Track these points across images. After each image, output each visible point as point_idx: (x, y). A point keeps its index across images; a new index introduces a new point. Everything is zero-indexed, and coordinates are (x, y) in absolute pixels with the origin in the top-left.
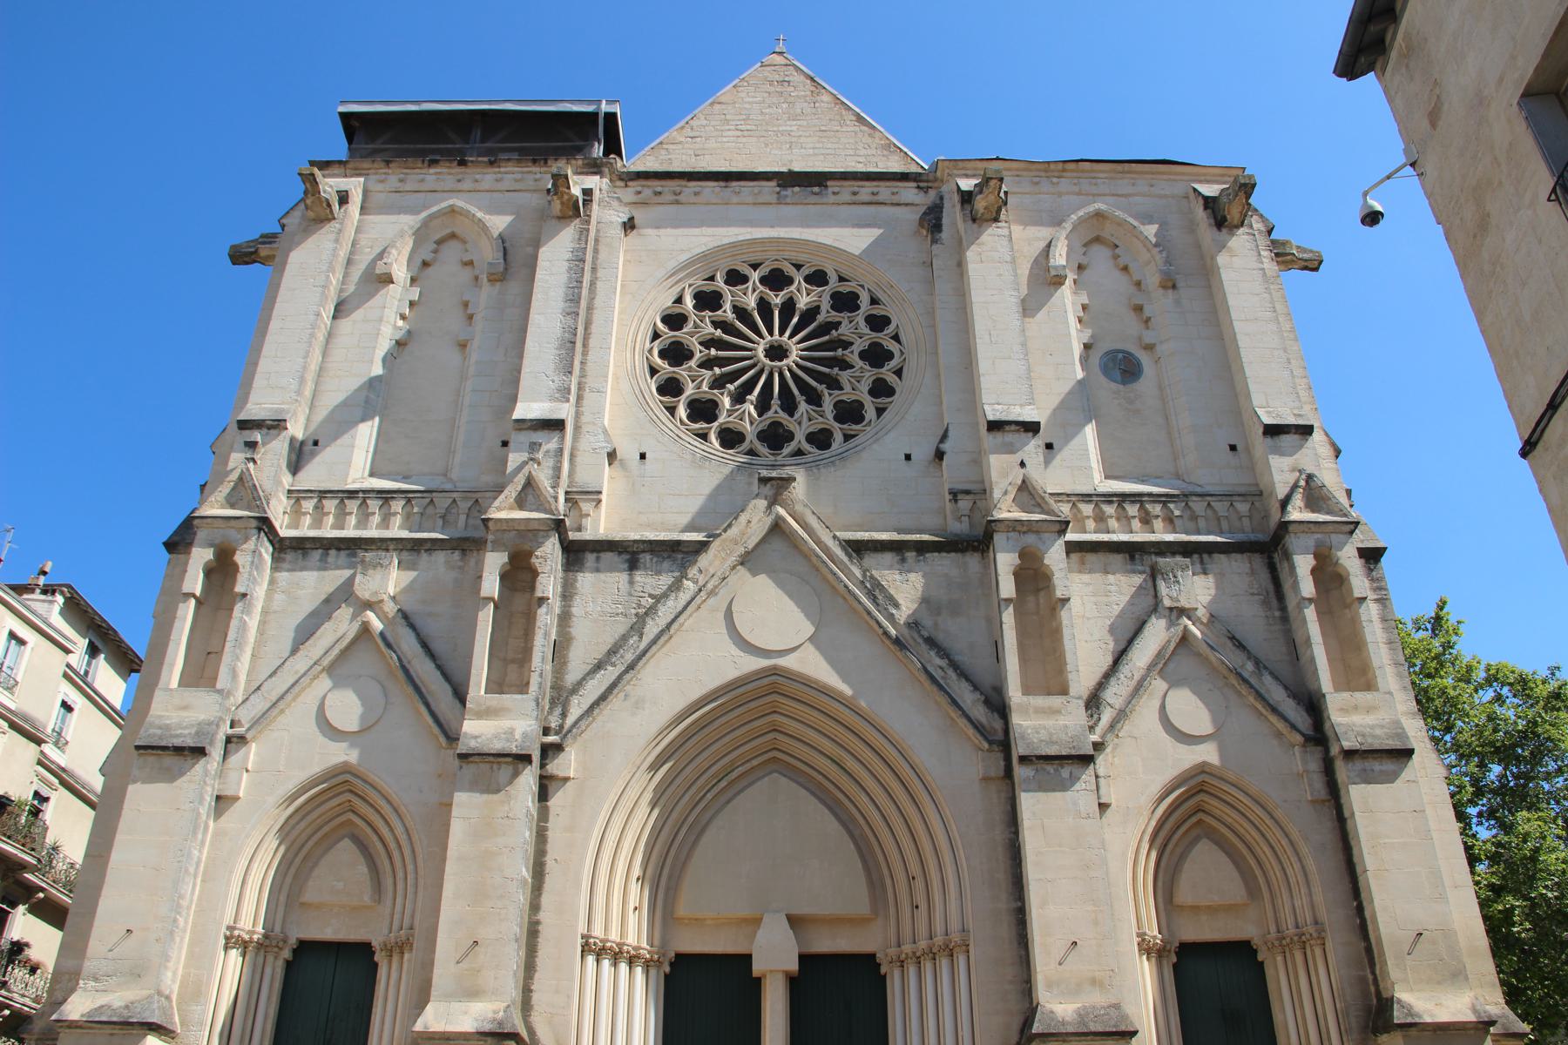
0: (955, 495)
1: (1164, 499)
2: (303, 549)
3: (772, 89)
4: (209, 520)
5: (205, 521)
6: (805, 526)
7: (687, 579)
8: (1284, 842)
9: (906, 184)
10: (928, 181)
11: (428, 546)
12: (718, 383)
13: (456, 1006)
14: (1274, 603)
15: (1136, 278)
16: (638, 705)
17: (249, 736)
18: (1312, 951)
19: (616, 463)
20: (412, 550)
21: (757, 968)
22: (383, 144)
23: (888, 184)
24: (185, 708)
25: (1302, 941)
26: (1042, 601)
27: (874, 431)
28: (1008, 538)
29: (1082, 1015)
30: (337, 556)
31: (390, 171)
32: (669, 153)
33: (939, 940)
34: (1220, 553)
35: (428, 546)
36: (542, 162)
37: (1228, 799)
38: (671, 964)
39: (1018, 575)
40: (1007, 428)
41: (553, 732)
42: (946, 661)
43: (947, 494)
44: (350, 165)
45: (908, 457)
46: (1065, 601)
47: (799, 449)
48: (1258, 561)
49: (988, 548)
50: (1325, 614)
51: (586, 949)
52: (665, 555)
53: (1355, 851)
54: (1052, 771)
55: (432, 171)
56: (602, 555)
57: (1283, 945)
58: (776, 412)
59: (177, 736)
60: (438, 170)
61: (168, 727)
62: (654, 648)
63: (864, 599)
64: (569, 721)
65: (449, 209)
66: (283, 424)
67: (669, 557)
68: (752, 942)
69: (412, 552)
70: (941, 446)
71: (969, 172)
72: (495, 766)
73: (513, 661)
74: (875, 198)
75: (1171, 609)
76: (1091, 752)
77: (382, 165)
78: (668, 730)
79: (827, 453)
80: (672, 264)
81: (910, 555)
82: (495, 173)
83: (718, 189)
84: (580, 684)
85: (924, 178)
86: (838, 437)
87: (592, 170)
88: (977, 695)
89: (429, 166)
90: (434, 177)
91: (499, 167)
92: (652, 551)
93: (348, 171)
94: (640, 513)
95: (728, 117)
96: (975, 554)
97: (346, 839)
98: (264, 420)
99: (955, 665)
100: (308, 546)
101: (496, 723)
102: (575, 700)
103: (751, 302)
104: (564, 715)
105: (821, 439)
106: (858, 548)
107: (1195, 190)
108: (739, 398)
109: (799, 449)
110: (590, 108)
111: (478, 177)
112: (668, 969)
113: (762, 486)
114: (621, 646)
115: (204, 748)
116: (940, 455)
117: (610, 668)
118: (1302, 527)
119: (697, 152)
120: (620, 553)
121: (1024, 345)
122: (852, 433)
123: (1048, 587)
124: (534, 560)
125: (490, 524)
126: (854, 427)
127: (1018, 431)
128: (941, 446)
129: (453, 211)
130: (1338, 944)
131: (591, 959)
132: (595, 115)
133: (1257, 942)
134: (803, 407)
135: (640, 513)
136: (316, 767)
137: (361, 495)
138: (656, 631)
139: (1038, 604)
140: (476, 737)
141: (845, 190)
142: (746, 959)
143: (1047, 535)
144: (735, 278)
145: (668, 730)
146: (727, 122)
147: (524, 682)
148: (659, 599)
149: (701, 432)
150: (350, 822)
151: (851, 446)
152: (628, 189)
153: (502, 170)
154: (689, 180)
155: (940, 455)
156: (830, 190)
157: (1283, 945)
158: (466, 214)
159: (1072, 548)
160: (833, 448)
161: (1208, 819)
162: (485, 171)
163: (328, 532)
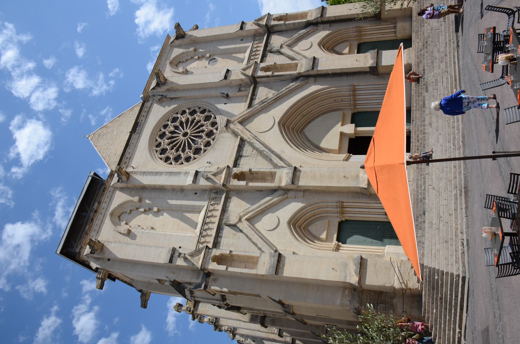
2: (216, 243)
3: (101, 138)
4: (203, 263)
5: (203, 265)
6: (242, 117)
8: (338, 32)
9: (145, 104)
10: (146, 100)
11: (224, 207)
12: (177, 150)
13: (361, 180)
14: (283, 32)
15: (135, 208)
17: (275, 249)
18: (345, 211)
20: (224, 212)
22: (89, 209)
23: (144, 108)
24: (264, 264)
25: (360, 31)
29: (372, 58)
31: (90, 234)
32: (112, 162)
33: (351, 93)
34: (268, 41)
35: (224, 207)
36: (105, 189)
37: (326, 42)
39: (239, 180)
40: (227, 75)
44: (83, 246)
46: (250, 170)
50: (252, 180)
53: (343, 18)
55: (95, 221)
56: (238, 164)
57: (360, 36)
58: (203, 135)
59: (274, 262)
60: (95, 219)
61: (270, 267)
63: (265, 103)
66: (174, 249)
69: (225, 212)
71: (148, 88)
72: (296, 176)
74: (147, 112)
75: (280, 48)
76: (277, 253)
77: (87, 235)
80: (150, 159)
81: (254, 97)
82: (103, 203)
83: (130, 147)
85: (145, 100)
86: (212, 141)
87: (112, 177)
89: (93, 222)
90: (97, 221)
91: (101, 202)
92: (240, 152)
94: (225, 162)
95: (106, 148)
98: (171, 254)
100: (216, 241)
101: (284, 178)
103: (172, 129)
105: (208, 144)
106: (250, 106)
107: (171, 43)
108: (183, 151)
110: (90, 178)
111: (102, 208)
118: (267, 22)
119: (115, 155)
120: (238, 159)
121: (204, 74)
124: (238, 173)
125: (224, 183)
130: (362, 24)
132: (93, 178)
133: (353, 112)
134: (204, 128)
135: (225, 162)
136: (288, 231)
138: (263, 147)
140: (287, 181)
141: (142, 118)
144: (165, 126)
146: (107, 148)
148: (254, 148)
150: (304, 228)
152: (131, 145)
153: (102, 201)
154: (124, 155)
156: (140, 122)
157: (360, 36)
158: (114, 210)
159: (262, 61)
160: (212, 144)
161: (330, 48)
162: (101, 206)
163: (213, 233)
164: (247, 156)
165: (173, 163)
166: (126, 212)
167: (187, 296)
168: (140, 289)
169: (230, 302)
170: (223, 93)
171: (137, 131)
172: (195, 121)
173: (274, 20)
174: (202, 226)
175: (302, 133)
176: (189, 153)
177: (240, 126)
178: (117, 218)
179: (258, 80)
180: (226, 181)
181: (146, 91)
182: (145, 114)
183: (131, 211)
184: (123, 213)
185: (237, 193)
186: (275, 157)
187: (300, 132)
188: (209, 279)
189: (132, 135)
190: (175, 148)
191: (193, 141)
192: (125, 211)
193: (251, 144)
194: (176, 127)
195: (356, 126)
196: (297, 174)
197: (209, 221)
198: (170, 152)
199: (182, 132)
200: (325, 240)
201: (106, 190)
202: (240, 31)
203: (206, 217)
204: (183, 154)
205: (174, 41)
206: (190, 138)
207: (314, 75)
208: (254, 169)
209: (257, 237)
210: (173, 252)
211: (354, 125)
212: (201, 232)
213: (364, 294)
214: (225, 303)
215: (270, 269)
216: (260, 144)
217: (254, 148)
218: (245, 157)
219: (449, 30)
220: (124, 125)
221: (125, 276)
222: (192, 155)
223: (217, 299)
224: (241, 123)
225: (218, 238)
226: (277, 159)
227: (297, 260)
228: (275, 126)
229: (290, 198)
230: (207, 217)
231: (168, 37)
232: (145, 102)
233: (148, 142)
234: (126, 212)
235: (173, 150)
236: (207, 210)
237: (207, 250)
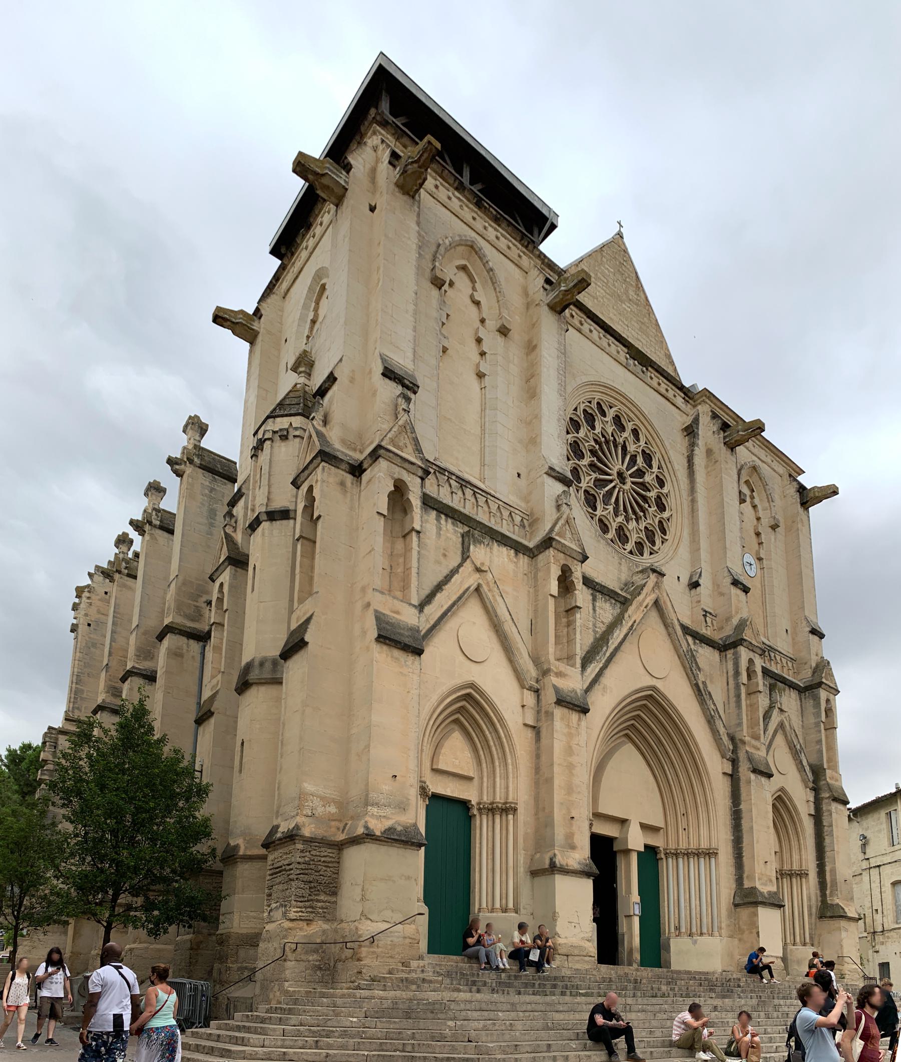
1: (464, 483)
4: (391, 455)
5: (388, 454)
10: (689, 397)
11: (499, 539)
24: (398, 613)
30: (446, 521)
52: (607, 598)
59: (400, 634)
65: (469, 243)
72: (571, 712)
89: (457, 189)
91: (499, 225)
93: (397, 143)
106: (686, 630)
115: (383, 374)
129: (472, 247)
136: (458, 681)
137: (447, 474)
148: (611, 628)
164: (594, 610)
165: (570, 436)
166: (474, 289)
167: (274, 422)
168: (263, 312)
169: (266, 532)
170: (700, 575)
171: (631, 362)
172: (646, 506)
173: (828, 701)
174: (457, 477)
175: (624, 739)
176: (588, 478)
177: (650, 600)
178: (463, 262)
179: (730, 653)
181: (709, 398)
182: (662, 389)
183: (477, 303)
184: (473, 281)
185: (525, 574)
186: (597, 670)
187: (627, 735)
188: (345, 471)
189: (624, 346)
190: (597, 447)
191: (610, 493)
192: (478, 285)
193: (617, 621)
194: (633, 459)
195: (639, 853)
196: (574, 712)
197: (467, 497)
198: (588, 434)
199: (628, 469)
200: (434, 767)
201: (523, 245)
202: (809, 629)
203: (476, 490)
204: (585, 466)
205: (795, 483)
206: (614, 487)
207: (738, 772)
208: (581, 619)
209: (445, 607)
210: (407, 383)
212: (445, 470)
213: (329, 851)
214: (264, 517)
215: (387, 623)
216: (619, 640)
217: (611, 628)
218: (593, 604)
219: (401, 1047)
220: (640, 333)
221: (300, 272)
223: (271, 497)
224: (656, 603)
225: (435, 512)
226: (593, 676)
227: (408, 692)
228: (648, 677)
229: (522, 694)
230: (475, 492)
231: (797, 470)
232: (685, 393)
233: (609, 382)
234: (474, 289)
235: (593, 443)
236: (489, 496)
237: (420, 473)
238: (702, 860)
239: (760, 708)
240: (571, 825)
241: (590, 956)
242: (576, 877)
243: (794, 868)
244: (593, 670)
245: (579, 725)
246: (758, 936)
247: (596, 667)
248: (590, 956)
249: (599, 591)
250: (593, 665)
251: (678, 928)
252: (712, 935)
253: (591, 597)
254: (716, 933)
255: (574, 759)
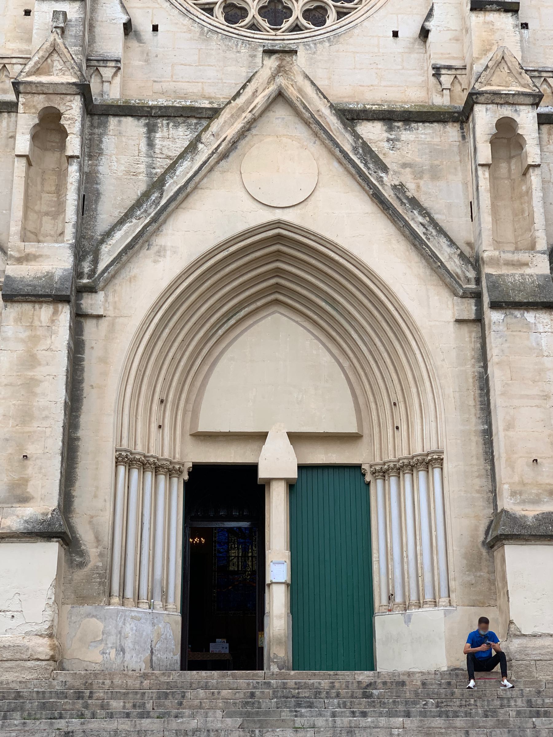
0: (437, 71)
7: (202, 143)
16: (161, 253)
19: (132, 34)
21: (262, 474)
26: (513, 167)
27: (366, 8)
28: (487, 109)
38: (190, 474)
41: (86, 276)
42: (428, 218)
43: (430, 68)
45: (395, 34)
47: (254, 24)
48: (280, 99)
49: (468, 118)
51: (119, 460)
52: (180, 120)
54: (519, 315)
62: (173, 205)
64: (101, 266)
67: (184, 123)
68: (259, 455)
70: (427, 24)
72: (37, 306)
73: (47, 214)
78: (186, 275)
79: (322, 30)
84: (108, 234)
86: (332, 14)
88: (453, 250)
94: (155, 81)
96: (455, 124)
97: (356, 129)
99: (434, 223)
102: (105, 248)
104: (95, 262)
109: (297, 25)
112: (186, 477)
113: (266, 58)
114: (144, 202)
115: (124, 24)
116: (424, 33)
117: (134, 221)
122: (345, 10)
123: (520, 154)
124: (62, 122)
126: (346, 5)
127: (498, 10)
128: (427, 24)
131: (122, 469)
138: (175, 188)
139: (509, 171)
142: (253, 468)
143: (522, 107)
145: (186, 275)
147: (59, 231)
149: (207, 6)
151: (343, 23)
155: (424, 33)
164: (151, 144)
180: (29, 89)
196: (44, 305)
211: (293, 474)
222: (253, 11)
238: (162, 478)
239: (349, 152)
240: (24, 467)
241: (38, 660)
242: (20, 542)
243: (152, 453)
244: (126, 234)
245: (53, 321)
246: (508, 601)
247: (136, 226)
248: (38, 660)
249: (160, 117)
250: (128, 225)
251: (391, 597)
252: (435, 604)
253: (145, 130)
254: (443, 600)
255: (39, 372)
